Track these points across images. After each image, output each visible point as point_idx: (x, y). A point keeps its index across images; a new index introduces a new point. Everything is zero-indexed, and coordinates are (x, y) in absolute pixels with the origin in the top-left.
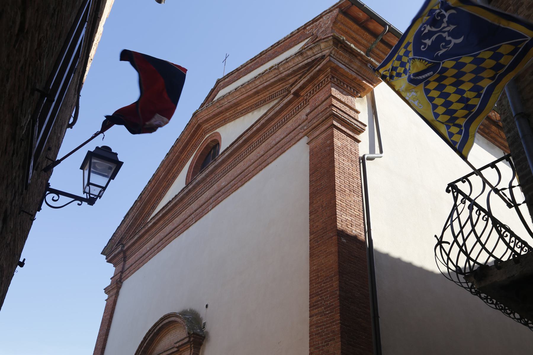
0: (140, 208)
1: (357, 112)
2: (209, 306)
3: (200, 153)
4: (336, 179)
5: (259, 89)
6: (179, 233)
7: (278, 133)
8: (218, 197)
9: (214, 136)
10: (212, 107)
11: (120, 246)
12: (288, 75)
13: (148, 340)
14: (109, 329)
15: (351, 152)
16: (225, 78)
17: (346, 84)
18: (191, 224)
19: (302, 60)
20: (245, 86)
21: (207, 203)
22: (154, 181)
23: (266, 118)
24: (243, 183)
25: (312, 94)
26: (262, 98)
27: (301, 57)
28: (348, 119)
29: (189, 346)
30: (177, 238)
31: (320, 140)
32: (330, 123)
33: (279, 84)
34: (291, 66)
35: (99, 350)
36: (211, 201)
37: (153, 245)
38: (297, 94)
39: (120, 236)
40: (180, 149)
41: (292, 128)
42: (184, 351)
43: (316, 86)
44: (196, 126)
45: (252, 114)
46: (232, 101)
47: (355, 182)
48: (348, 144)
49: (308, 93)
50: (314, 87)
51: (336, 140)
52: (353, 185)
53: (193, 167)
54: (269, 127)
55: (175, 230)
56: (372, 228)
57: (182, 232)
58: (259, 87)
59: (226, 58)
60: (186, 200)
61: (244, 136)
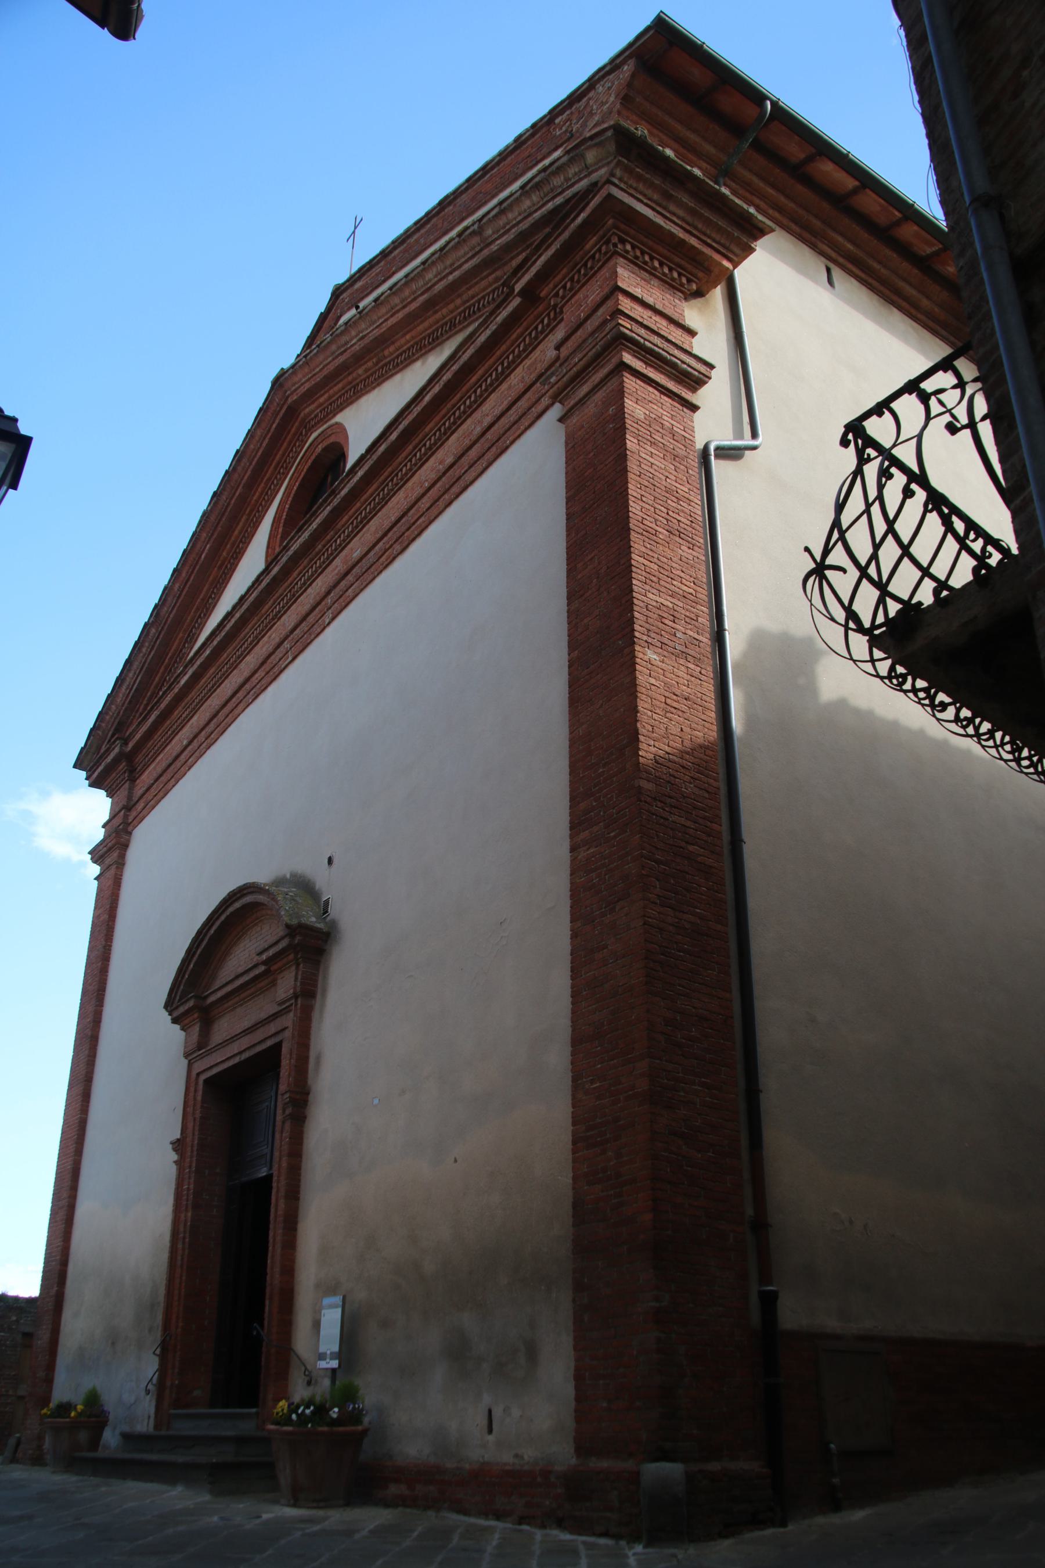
0: (158, 642)
1: (692, 333)
2: (335, 861)
3: (297, 484)
4: (630, 502)
5: (435, 292)
6: (255, 692)
7: (487, 405)
8: (345, 589)
9: (330, 435)
10: (321, 357)
11: (116, 743)
12: (507, 248)
13: (197, 956)
14: (110, 946)
15: (674, 435)
16: (353, 280)
17: (657, 259)
18: (283, 666)
19: (541, 203)
20: (400, 290)
21: (319, 607)
22: (187, 568)
23: (455, 368)
24: (406, 543)
25: (569, 290)
26: (444, 317)
27: (538, 193)
28: (663, 350)
29: (292, 956)
30: (251, 707)
31: (591, 408)
32: (614, 361)
33: (485, 274)
34: (512, 221)
35: (92, 994)
36: (329, 601)
37: (196, 730)
38: (530, 294)
39: (115, 718)
40: (246, 477)
41: (521, 387)
42: (281, 970)
43: (577, 268)
44: (283, 411)
45: (423, 364)
46: (370, 335)
47: (683, 511)
48: (665, 413)
49: (559, 290)
50: (573, 273)
51: (630, 403)
52: (679, 518)
53: (282, 521)
54: (464, 389)
55: (246, 686)
56: (727, 625)
57: (262, 688)
58: (436, 287)
59: (355, 228)
60: (267, 607)
61: (401, 420)
